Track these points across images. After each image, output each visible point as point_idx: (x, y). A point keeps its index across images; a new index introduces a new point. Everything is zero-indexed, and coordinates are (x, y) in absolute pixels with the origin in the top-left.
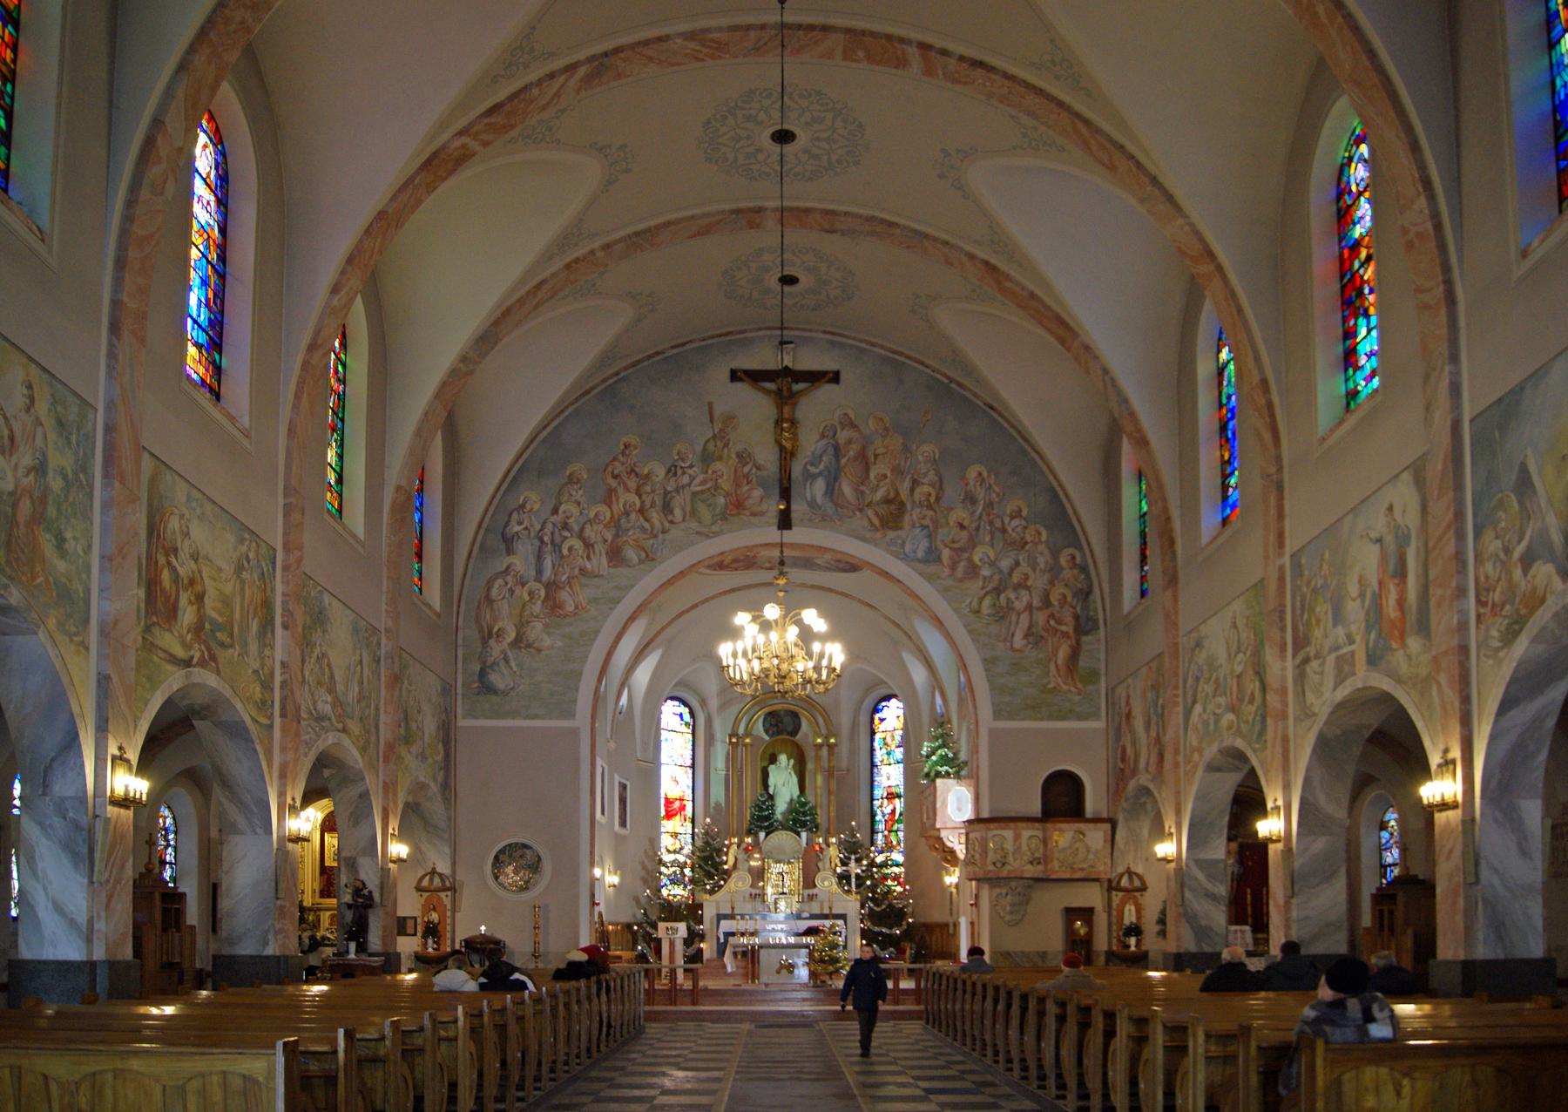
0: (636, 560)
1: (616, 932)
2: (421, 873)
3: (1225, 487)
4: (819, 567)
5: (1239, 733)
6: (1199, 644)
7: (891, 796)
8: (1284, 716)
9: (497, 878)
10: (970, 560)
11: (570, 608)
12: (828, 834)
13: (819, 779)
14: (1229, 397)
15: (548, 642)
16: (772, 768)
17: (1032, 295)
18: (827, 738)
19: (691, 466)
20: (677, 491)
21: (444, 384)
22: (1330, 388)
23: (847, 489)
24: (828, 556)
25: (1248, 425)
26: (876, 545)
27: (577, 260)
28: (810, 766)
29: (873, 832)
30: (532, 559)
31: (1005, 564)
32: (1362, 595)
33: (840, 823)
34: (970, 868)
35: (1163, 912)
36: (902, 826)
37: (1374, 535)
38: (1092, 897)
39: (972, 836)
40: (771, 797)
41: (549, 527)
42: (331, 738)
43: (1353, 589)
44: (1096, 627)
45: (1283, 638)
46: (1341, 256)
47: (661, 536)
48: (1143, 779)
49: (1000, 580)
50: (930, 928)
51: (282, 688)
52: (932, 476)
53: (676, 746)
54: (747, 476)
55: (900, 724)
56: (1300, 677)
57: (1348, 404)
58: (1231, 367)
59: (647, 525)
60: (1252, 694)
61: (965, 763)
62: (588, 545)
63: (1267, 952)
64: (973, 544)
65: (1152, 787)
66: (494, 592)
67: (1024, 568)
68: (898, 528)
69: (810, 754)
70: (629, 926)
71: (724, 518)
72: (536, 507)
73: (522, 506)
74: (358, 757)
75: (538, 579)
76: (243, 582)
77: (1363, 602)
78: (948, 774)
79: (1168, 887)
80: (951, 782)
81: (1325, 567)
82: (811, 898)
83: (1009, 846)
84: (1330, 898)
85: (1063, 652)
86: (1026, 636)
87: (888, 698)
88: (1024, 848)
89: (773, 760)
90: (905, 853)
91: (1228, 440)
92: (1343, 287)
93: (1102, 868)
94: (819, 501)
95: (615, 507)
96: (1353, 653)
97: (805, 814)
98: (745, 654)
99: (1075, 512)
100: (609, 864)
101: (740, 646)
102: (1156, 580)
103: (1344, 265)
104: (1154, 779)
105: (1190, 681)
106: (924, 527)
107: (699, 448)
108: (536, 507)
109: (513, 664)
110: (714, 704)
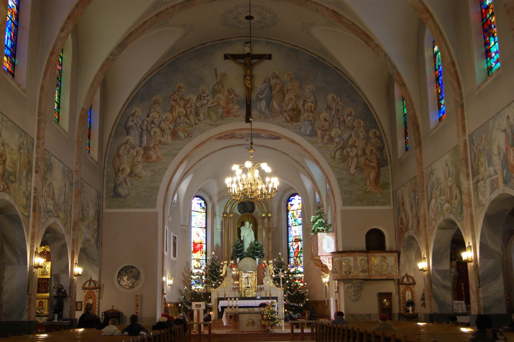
0: (183, 137)
1: (171, 307)
2: (85, 281)
3: (439, 104)
4: (263, 138)
5: (451, 212)
6: (432, 173)
7: (297, 240)
8: (470, 205)
9: (119, 282)
10: (330, 135)
11: (154, 158)
12: (268, 259)
13: (264, 233)
14: (439, 66)
15: (144, 173)
16: (242, 228)
17: (353, 24)
18: (267, 214)
19: (207, 96)
20: (201, 106)
21: (103, 65)
22: (480, 66)
23: (275, 105)
24: (267, 133)
25: (446, 79)
26: (289, 129)
27: (161, 12)
28: (260, 227)
29: (289, 257)
30: (138, 137)
31: (345, 136)
32: (499, 154)
33: (274, 253)
34: (335, 275)
35: (423, 295)
36: (302, 255)
37: (502, 128)
38: (390, 287)
39: (335, 259)
40: (242, 242)
41: (146, 123)
42: (52, 221)
43: (495, 151)
44: (387, 164)
45: (467, 171)
46: (482, 12)
47: (194, 126)
48: (411, 233)
49: (344, 143)
50: (317, 303)
51: (34, 199)
52: (312, 98)
53: (198, 218)
54: (232, 99)
55: (300, 207)
56: (476, 188)
57: (488, 72)
58: (439, 54)
59: (188, 122)
60: (456, 195)
61: (331, 225)
62: (163, 131)
63: (471, 313)
64: (331, 127)
65: (415, 236)
66: (121, 152)
67: (354, 138)
68: (298, 121)
69: (259, 221)
70: (176, 304)
71: (222, 118)
72: (140, 114)
73: (134, 114)
74: (62, 227)
75: (140, 146)
76: (21, 154)
77: (500, 156)
78: (323, 231)
79: (425, 283)
80: (324, 234)
81: (483, 141)
82: (261, 289)
83: (352, 264)
84: (497, 288)
85: (373, 175)
86: (356, 168)
87: (294, 195)
88: (359, 265)
89: (243, 224)
90: (304, 267)
91: (439, 84)
92: (483, 25)
93: (395, 274)
94: (263, 110)
95: (174, 114)
96: (497, 178)
97: (258, 249)
98: (237, 182)
99: (375, 114)
100: (168, 274)
101: (235, 179)
102: (412, 144)
103: (483, 16)
104: (415, 233)
105: (429, 189)
106: (309, 121)
107: (211, 88)
108: (140, 114)
109: (129, 184)
110: (215, 199)
